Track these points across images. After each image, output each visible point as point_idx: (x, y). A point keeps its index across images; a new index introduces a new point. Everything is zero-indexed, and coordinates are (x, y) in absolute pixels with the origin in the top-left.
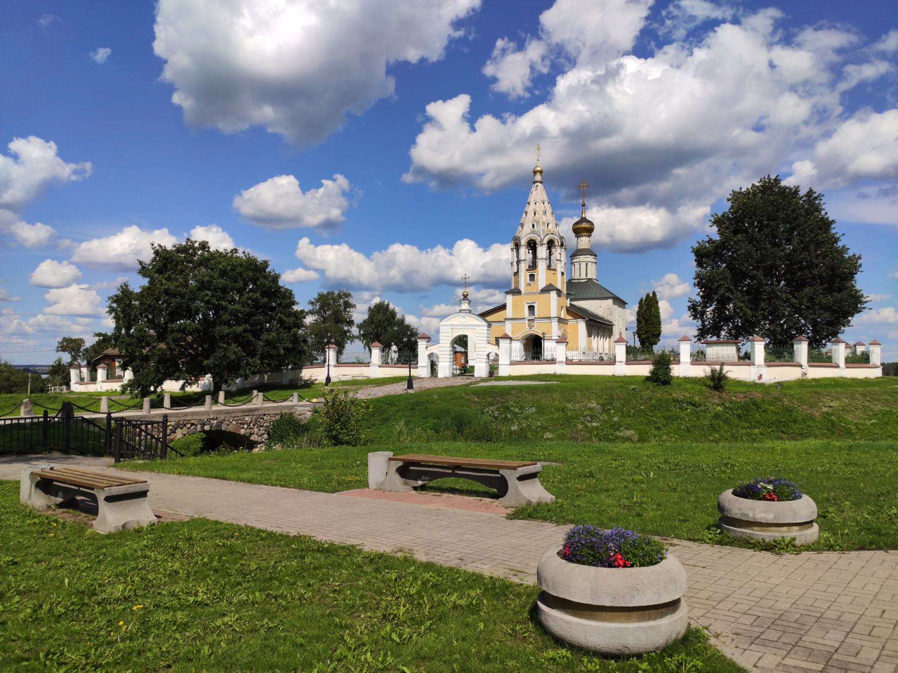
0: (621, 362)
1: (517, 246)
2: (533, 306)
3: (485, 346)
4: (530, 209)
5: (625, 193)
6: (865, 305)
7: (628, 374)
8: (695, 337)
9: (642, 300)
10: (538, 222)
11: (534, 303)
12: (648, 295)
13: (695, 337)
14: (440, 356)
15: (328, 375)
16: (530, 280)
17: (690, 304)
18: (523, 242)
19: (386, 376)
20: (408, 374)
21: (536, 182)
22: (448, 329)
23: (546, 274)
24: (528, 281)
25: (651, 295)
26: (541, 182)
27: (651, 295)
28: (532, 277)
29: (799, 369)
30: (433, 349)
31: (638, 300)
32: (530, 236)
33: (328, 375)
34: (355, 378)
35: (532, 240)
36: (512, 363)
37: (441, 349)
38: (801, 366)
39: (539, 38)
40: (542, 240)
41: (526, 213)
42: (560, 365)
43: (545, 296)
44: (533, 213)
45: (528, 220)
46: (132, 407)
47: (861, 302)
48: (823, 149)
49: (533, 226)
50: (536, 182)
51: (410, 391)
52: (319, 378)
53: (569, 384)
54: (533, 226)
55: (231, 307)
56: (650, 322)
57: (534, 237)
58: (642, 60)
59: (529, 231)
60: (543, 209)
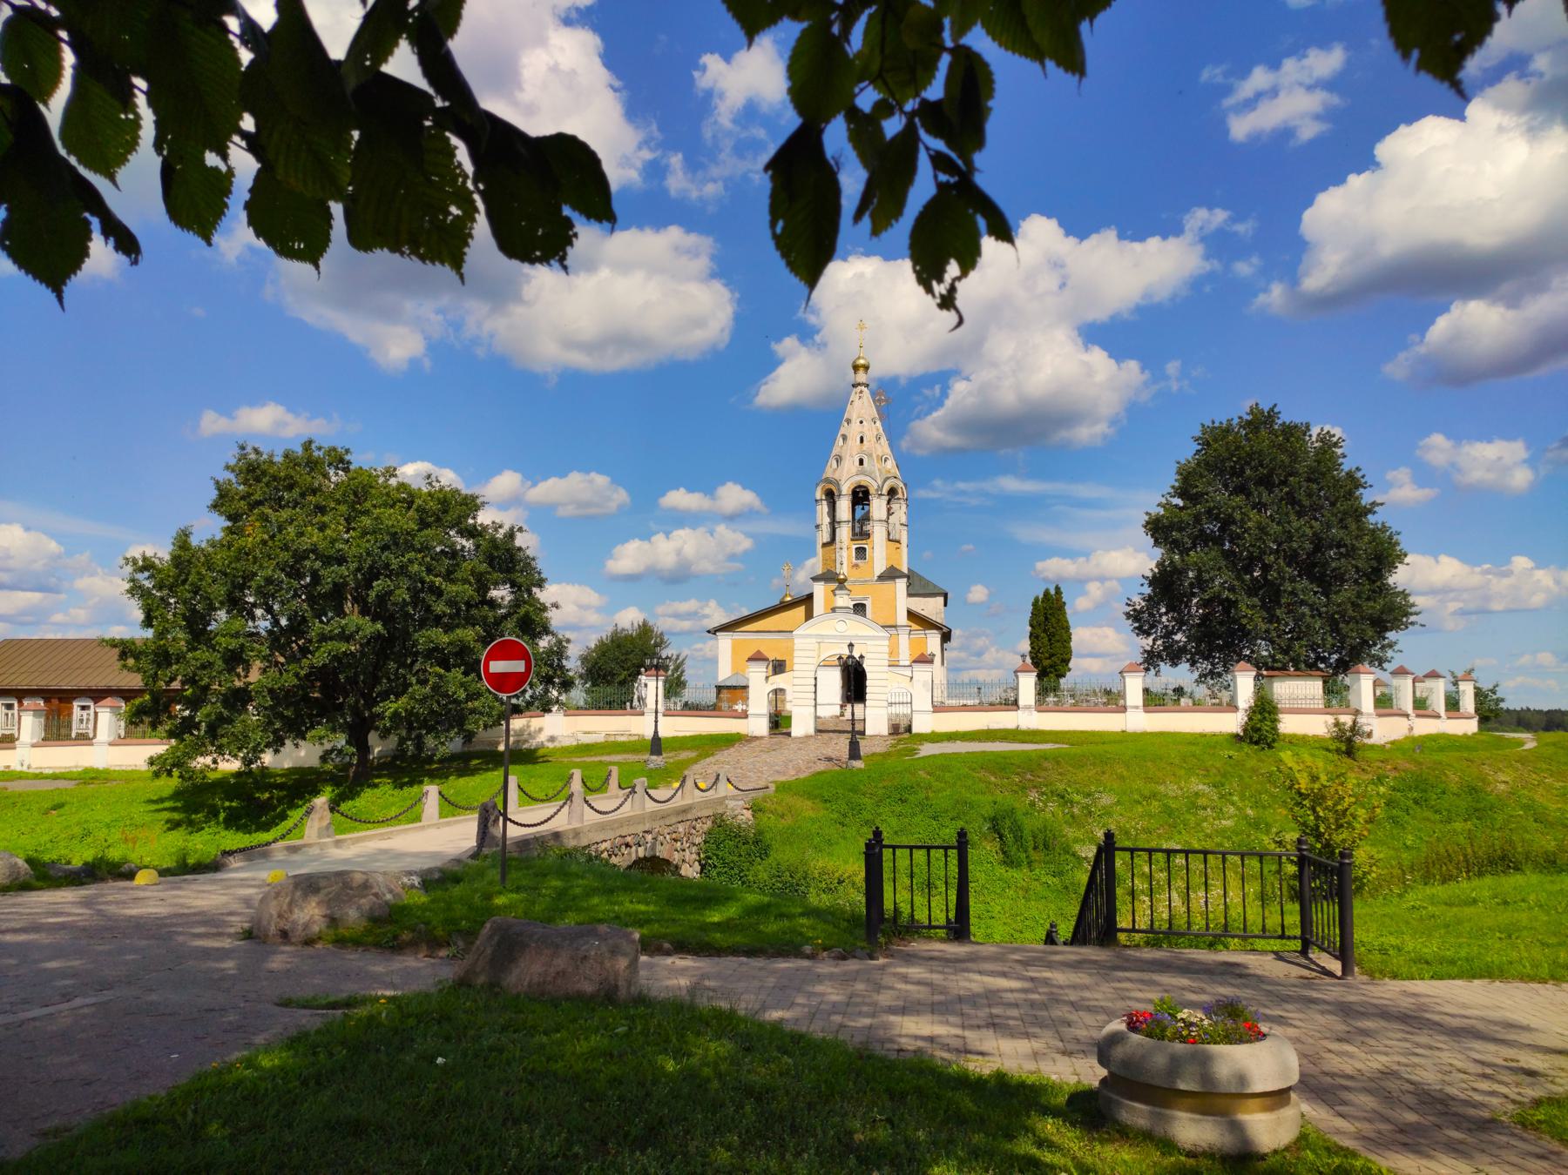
0: (1137, 707)
2: (863, 606)
3: (885, 676)
4: (853, 431)
6: (1412, 619)
9: (1037, 600)
10: (870, 456)
11: (865, 599)
12: (1047, 593)
15: (656, 732)
16: (857, 558)
17: (1129, 609)
18: (846, 489)
20: (649, 733)
21: (859, 384)
23: (887, 548)
24: (854, 561)
25: (1053, 592)
26: (867, 386)
27: (1053, 592)
28: (861, 552)
29: (1405, 719)
30: (779, 681)
31: (1032, 600)
33: (656, 732)
34: (612, 739)
35: (860, 486)
36: (938, 708)
37: (797, 681)
38: (1407, 716)
41: (845, 438)
42: (1027, 713)
43: (888, 585)
45: (850, 451)
47: (1407, 614)
49: (861, 462)
50: (859, 384)
51: (858, 764)
54: (861, 462)
55: (452, 589)
56: (1057, 637)
58: (173, 224)
59: (854, 470)
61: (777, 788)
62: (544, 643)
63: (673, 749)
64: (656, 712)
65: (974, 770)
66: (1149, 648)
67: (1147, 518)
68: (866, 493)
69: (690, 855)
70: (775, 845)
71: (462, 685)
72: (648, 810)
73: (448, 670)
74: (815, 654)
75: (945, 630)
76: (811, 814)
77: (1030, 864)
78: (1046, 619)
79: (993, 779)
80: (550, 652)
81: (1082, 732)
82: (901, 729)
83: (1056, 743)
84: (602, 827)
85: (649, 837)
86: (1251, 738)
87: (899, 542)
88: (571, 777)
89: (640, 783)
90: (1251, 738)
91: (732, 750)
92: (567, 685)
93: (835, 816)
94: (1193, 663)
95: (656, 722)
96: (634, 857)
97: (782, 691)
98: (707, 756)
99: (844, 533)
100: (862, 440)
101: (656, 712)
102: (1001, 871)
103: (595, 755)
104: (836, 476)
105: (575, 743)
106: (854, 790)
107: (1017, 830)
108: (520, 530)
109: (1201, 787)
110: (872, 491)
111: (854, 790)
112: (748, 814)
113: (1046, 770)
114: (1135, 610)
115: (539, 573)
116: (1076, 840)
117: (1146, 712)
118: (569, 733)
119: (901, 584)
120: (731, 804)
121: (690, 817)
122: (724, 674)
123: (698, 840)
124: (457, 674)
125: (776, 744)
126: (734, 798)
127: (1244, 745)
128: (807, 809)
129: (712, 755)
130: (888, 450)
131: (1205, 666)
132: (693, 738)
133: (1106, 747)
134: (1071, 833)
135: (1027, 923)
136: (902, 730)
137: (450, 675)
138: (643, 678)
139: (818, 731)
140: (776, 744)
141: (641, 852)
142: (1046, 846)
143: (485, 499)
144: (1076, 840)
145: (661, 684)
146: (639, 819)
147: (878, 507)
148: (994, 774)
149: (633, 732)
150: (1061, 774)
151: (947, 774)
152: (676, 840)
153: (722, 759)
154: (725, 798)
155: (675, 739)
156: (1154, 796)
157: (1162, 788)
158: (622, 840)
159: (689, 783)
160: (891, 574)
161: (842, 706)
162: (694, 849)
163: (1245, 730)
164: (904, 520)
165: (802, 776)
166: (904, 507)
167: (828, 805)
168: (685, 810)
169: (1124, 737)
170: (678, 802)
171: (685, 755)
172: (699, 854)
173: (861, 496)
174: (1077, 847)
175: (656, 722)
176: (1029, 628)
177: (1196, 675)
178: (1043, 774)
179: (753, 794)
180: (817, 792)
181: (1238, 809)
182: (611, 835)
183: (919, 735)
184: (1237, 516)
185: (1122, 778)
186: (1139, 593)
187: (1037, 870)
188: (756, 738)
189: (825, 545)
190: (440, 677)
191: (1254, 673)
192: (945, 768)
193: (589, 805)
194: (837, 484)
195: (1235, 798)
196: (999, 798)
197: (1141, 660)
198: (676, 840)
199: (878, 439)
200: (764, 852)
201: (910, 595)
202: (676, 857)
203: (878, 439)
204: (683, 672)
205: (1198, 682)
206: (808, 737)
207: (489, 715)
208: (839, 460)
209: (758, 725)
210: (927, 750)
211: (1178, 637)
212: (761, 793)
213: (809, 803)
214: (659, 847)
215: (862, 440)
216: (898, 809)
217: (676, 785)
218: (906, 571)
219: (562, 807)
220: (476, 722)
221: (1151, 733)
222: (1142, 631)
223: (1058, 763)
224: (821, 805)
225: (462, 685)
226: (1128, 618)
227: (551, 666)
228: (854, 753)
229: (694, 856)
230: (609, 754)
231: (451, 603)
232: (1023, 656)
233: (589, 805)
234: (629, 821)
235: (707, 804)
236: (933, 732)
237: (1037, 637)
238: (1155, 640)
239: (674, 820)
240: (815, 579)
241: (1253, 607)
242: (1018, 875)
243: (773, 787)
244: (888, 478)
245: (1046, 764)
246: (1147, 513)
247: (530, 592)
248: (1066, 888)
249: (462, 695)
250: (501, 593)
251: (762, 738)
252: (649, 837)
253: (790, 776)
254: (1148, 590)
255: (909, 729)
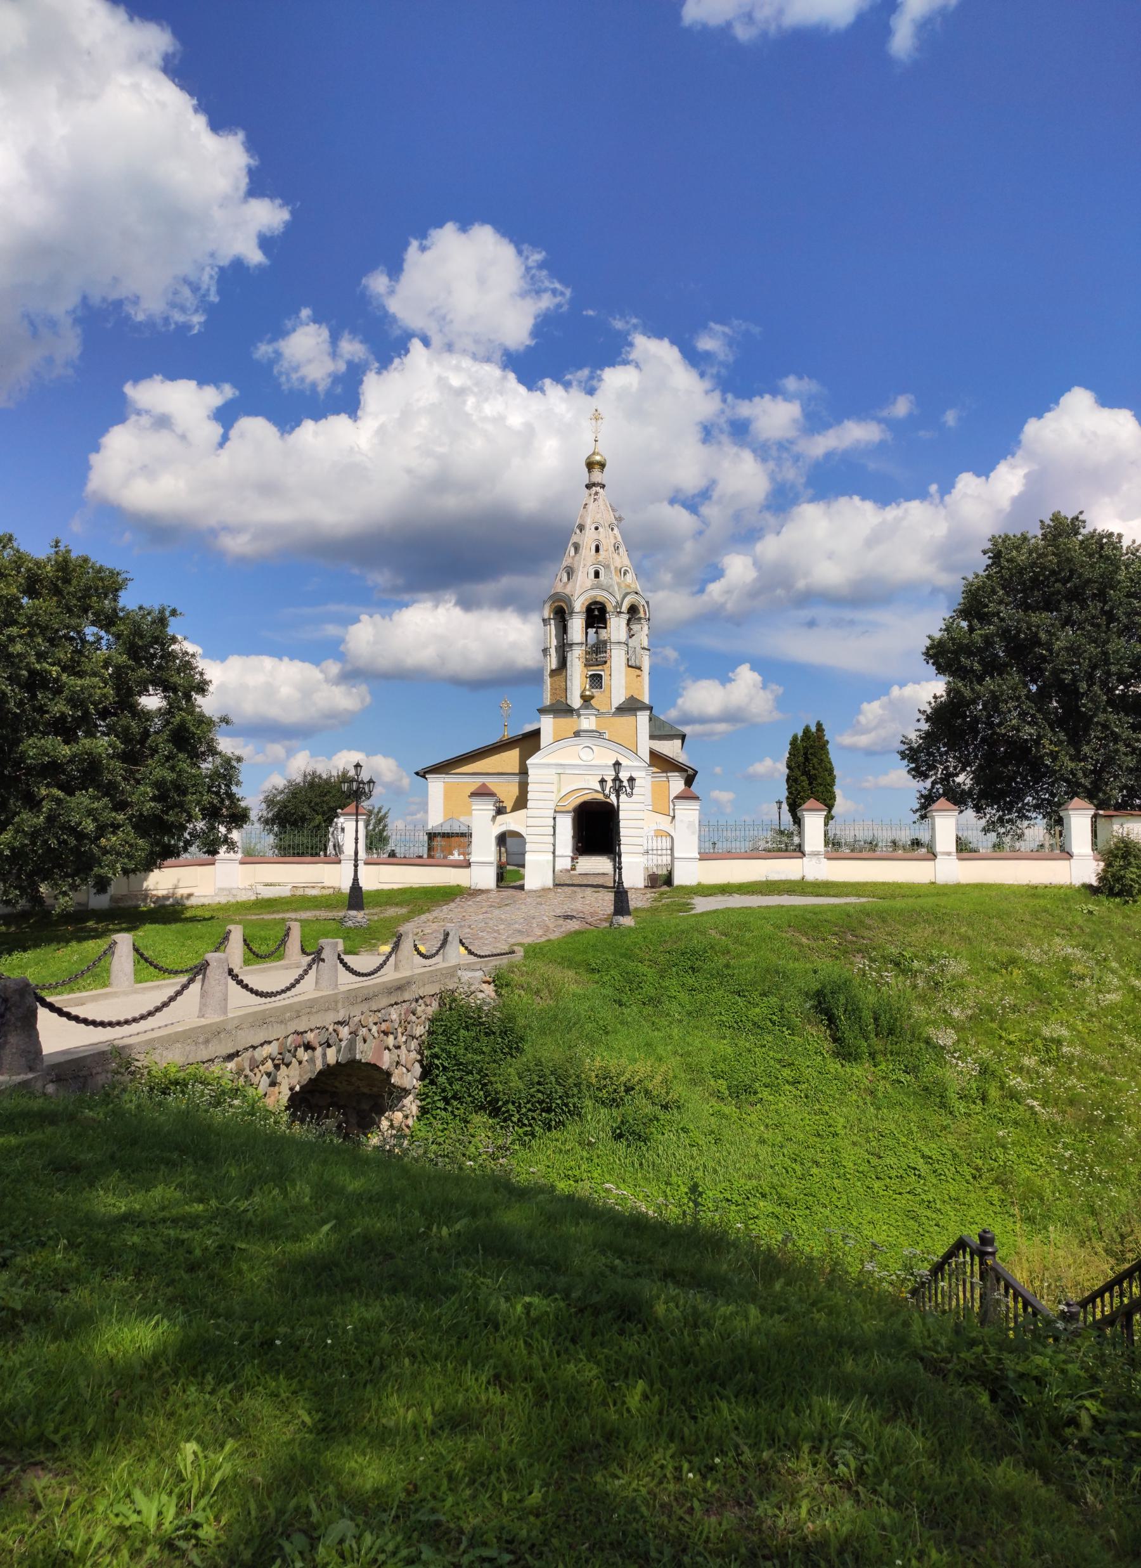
0: (949, 854)
1: (561, 615)
5: (489, 588)
7: (964, 880)
8: (915, 812)
9: (795, 738)
10: (607, 567)
12: (807, 731)
13: (915, 812)
14: (528, 839)
15: (356, 879)
16: (592, 687)
19: (386, 887)
22: (550, 774)
23: (627, 675)
25: (813, 729)
27: (813, 729)
28: (596, 680)
30: (512, 822)
31: (790, 738)
32: (594, 593)
33: (356, 879)
34: (300, 892)
35: (596, 603)
37: (531, 822)
39: (391, 279)
40: (619, 605)
41: (577, 547)
42: (814, 860)
43: (626, 720)
44: (593, 548)
46: (64, 984)
48: (770, 547)
49: (597, 575)
50: (594, 485)
51: (627, 921)
52: (196, 892)
53: (911, 901)
54: (597, 575)
57: (600, 595)
60: (613, 541)
61: (526, 952)
62: (207, 766)
63: (378, 904)
64: (356, 860)
65: (779, 927)
66: (925, 792)
67: (928, 642)
68: (603, 609)
69: (410, 1055)
70: (531, 1036)
71: (90, 812)
72: (343, 988)
73: (71, 793)
74: (554, 788)
75: (690, 772)
76: (573, 988)
77: (872, 1055)
78: (807, 759)
79: (804, 940)
80: (215, 775)
81: (884, 884)
82: (661, 881)
83: (859, 896)
84: (262, 1020)
85: (344, 1032)
86: (1111, 889)
87: (639, 668)
88: (226, 937)
89: (332, 946)
90: (1111, 889)
91: (452, 905)
92: (239, 818)
93: (608, 991)
94: (978, 809)
95: (356, 871)
96: (319, 1065)
97: (517, 835)
98: (422, 912)
99: (576, 658)
100: (597, 549)
101: (356, 860)
102: (834, 1066)
103: (278, 912)
104: (568, 591)
105: (253, 898)
106: (628, 955)
107: (854, 1011)
108: (174, 613)
109: (1070, 950)
110: (609, 608)
111: (628, 955)
112: (489, 990)
113: (869, 928)
114: (911, 749)
115: (202, 674)
116: (928, 1022)
117: (960, 859)
118: (246, 884)
119: (643, 718)
120: (466, 976)
121: (407, 996)
122: (436, 819)
123: (419, 1030)
124: (83, 799)
125: (508, 898)
126: (469, 968)
127: (1102, 898)
128: (570, 982)
129: (429, 911)
130: (626, 561)
131: (992, 812)
132: (402, 891)
133: (919, 901)
134: (920, 1012)
135: (885, 1141)
136: (660, 883)
137: (72, 801)
138: (340, 821)
139: (556, 885)
140: (508, 898)
141: (332, 1056)
142: (891, 1032)
143: (128, 576)
144: (928, 1022)
145: (361, 824)
146: (329, 1004)
147: (617, 627)
148: (806, 934)
149: (327, 884)
150: (890, 934)
151: (748, 935)
152: (386, 1033)
153: (442, 915)
154: (458, 967)
155: (379, 893)
156: (1013, 961)
157: (1023, 953)
158: (299, 1039)
159: (406, 946)
160: (631, 707)
161: (573, 859)
162: (414, 1044)
163: (1101, 879)
164: (645, 644)
165: (553, 937)
166: (646, 628)
167: (597, 976)
168: (400, 987)
169: (936, 890)
170: (389, 975)
171: (391, 912)
172: (420, 1053)
173: (596, 616)
174: (931, 1031)
175: (356, 871)
176: (787, 771)
177: (983, 822)
178: (866, 933)
179: (495, 962)
180: (579, 958)
181: (1124, 979)
182: (278, 1031)
183: (682, 888)
184: (1043, 636)
185: (966, 939)
186: (914, 730)
187: (883, 1067)
188: (481, 892)
189: (553, 673)
190: (59, 801)
191: (1092, 812)
192: (744, 926)
193: (240, 982)
194: (568, 600)
195: (1114, 965)
196: (818, 964)
197: (918, 806)
198: (386, 1033)
199: (617, 548)
200: (514, 1048)
201: (652, 737)
202: (386, 1061)
203: (617, 548)
204: (385, 826)
205: (986, 830)
206: (545, 890)
207: (130, 856)
208: (570, 572)
209: (483, 876)
210: (702, 905)
211: (960, 779)
212: (504, 961)
213: (571, 973)
214: (360, 1046)
215: (597, 549)
216: (690, 981)
217: (386, 949)
218: (646, 700)
219: (185, 987)
220: (112, 866)
221: (968, 885)
222: (919, 773)
223: (884, 921)
224: (586, 976)
225: (90, 812)
226: (903, 758)
227: (217, 794)
228: (621, 903)
229: (414, 1055)
230: (295, 910)
231: (73, 702)
232: (780, 803)
233: (240, 982)
234: (311, 1006)
235: (433, 977)
236: (699, 884)
237: (796, 780)
238: (934, 783)
239: (384, 1002)
240: (543, 711)
241: (1059, 743)
242: (859, 1071)
243: (520, 952)
244: (627, 594)
245: (868, 921)
246: (929, 637)
247: (188, 697)
248: (926, 1089)
249: (90, 826)
250: (152, 702)
251: (487, 891)
252: (344, 1032)
253: (536, 936)
254: (925, 726)
255: (668, 880)
